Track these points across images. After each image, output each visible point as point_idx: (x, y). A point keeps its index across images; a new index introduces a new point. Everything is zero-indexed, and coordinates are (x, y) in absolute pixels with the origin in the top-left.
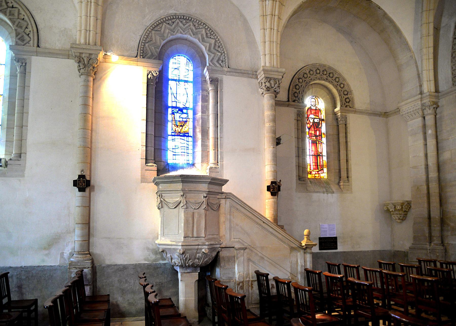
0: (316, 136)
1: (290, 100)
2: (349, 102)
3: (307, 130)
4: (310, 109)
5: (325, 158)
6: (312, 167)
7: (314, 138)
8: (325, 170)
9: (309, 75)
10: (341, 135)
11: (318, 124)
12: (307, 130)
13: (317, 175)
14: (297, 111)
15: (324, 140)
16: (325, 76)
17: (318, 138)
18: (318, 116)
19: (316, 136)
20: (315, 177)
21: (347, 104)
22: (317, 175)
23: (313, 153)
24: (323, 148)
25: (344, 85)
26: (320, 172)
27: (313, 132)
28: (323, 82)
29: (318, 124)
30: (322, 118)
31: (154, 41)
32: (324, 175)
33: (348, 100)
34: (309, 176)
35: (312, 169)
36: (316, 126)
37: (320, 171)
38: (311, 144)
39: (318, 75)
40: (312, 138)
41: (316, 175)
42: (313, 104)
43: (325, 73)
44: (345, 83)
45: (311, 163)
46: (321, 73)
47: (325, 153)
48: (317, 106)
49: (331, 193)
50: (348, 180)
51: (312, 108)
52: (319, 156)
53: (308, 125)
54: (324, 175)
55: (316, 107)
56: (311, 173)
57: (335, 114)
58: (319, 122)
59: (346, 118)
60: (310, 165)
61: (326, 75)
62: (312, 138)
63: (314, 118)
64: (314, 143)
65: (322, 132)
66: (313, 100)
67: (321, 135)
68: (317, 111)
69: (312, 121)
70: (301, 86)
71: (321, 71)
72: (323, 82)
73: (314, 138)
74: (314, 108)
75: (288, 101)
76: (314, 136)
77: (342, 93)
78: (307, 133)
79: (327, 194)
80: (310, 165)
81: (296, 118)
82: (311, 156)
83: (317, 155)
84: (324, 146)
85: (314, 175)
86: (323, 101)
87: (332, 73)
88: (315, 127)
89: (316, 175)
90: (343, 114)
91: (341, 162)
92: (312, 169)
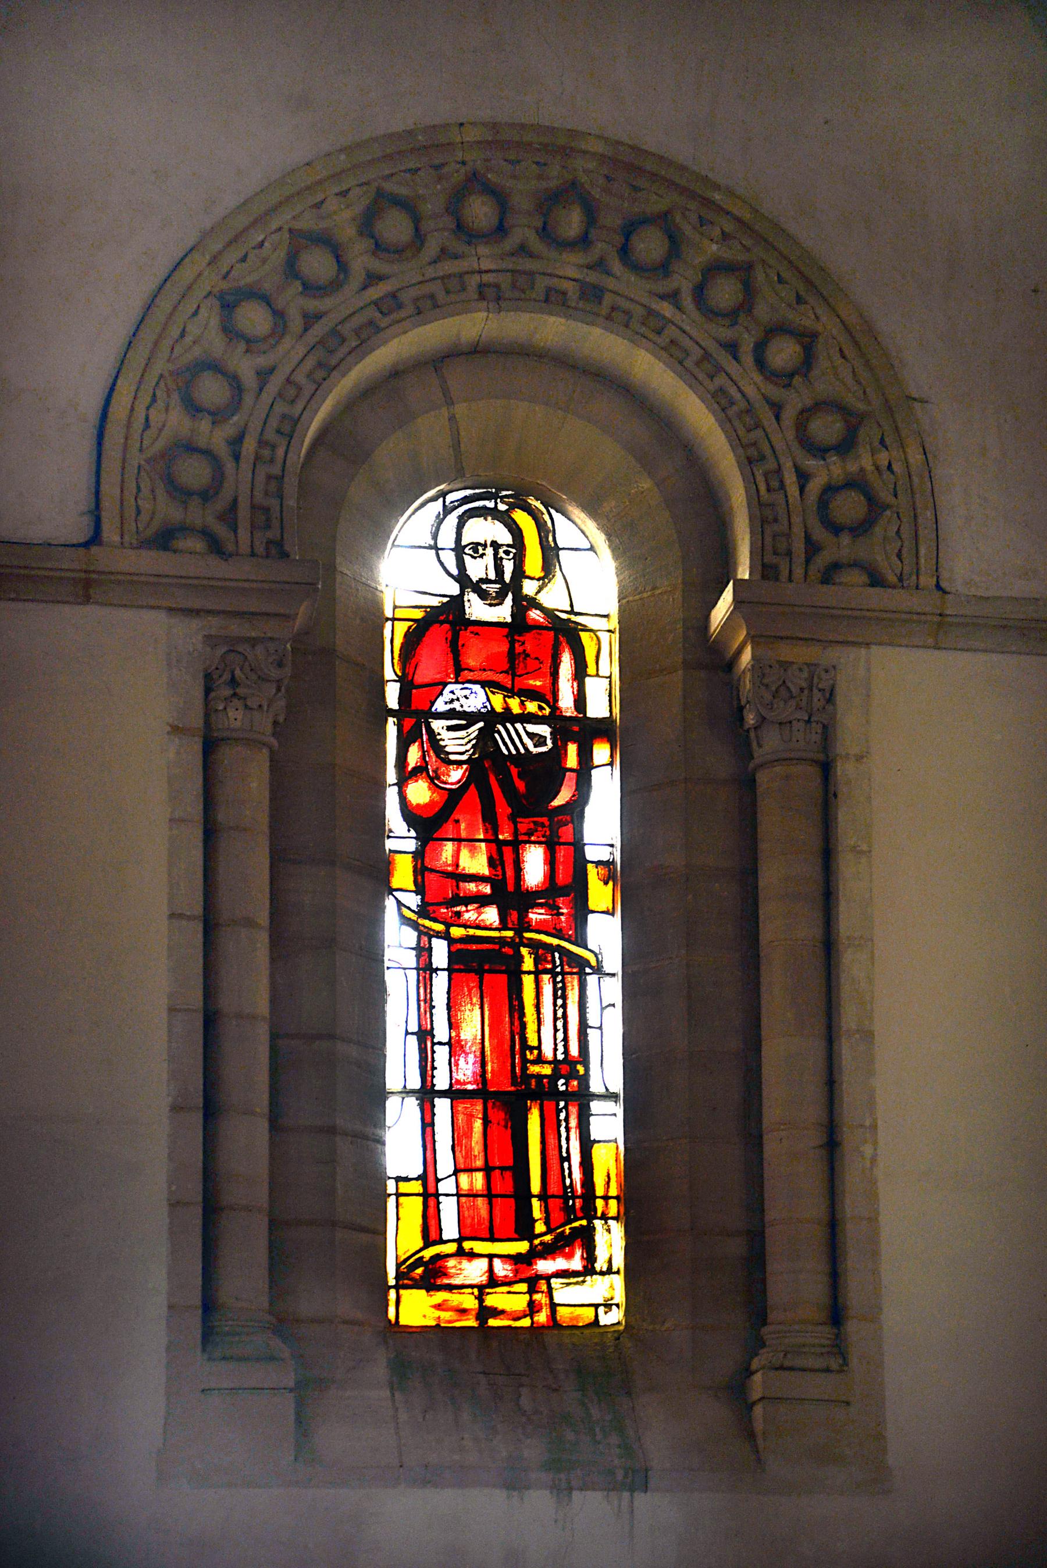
0: (510, 896)
1: (110, 533)
2: (861, 529)
3: (401, 839)
4: (446, 620)
5: (608, 1124)
6: (449, 1209)
7: (491, 915)
8: (611, 1242)
9: (360, 260)
10: (772, 875)
11: (545, 771)
12: (401, 839)
13: (510, 1300)
14: (211, 640)
15: (605, 935)
16: (570, 267)
17: (536, 916)
18: (550, 697)
19: (510, 896)
20: (485, 1312)
21: (844, 547)
22: (510, 1300)
23: (467, 1070)
24: (596, 1024)
25: (808, 340)
26: (544, 1266)
27: (475, 862)
28: (552, 329)
29: (545, 771)
30: (598, 707)
31: (333, 362)
32: (594, 1294)
33: (849, 507)
34: (416, 1309)
35: (450, 1228)
36: (519, 793)
37: (548, 1251)
38: (441, 983)
39: (485, 258)
40: (456, 920)
41: (496, 1299)
42: (478, 568)
43: (571, 223)
44: (828, 325)
45: (445, 1164)
46: (523, 232)
47: (607, 1070)
48: (529, 588)
49: (612, 1487)
50: (839, 1348)
51: (477, 609)
52: (544, 1092)
53: (419, 793)
54: (594, 1294)
55: (523, 604)
56: (429, 1275)
57: (712, 658)
58: (558, 753)
59: (830, 698)
60: (430, 1197)
61: (584, 241)
62: (456, 920)
63: (491, 719)
64: (484, 968)
65: (592, 854)
66: (484, 530)
67: (568, 888)
68: (539, 642)
69: (457, 743)
70: (264, 375)
71: (521, 202)
72: (552, 329)
73: (491, 915)
74: (503, 613)
75: (95, 539)
76: (482, 901)
77: (782, 437)
78: (403, 874)
79: (563, 1491)
80: (430, 1197)
81: (196, 719)
82: (443, 1107)
83: (518, 1093)
84: (606, 998)
85: (469, 1302)
86: (599, 538)
87: (663, 219)
88: (503, 809)
89: (496, 1299)
90: (787, 652)
91: (771, 1148)
92: (450, 1228)
